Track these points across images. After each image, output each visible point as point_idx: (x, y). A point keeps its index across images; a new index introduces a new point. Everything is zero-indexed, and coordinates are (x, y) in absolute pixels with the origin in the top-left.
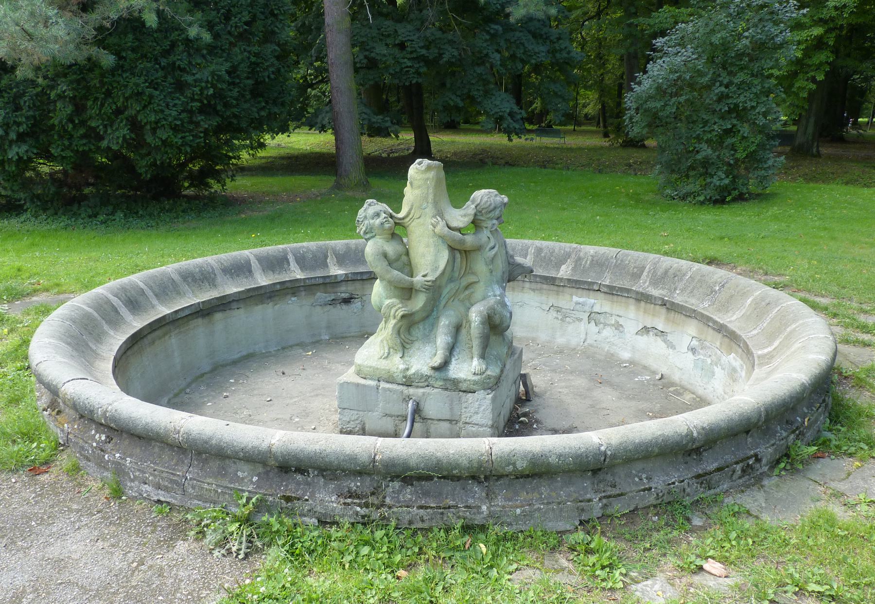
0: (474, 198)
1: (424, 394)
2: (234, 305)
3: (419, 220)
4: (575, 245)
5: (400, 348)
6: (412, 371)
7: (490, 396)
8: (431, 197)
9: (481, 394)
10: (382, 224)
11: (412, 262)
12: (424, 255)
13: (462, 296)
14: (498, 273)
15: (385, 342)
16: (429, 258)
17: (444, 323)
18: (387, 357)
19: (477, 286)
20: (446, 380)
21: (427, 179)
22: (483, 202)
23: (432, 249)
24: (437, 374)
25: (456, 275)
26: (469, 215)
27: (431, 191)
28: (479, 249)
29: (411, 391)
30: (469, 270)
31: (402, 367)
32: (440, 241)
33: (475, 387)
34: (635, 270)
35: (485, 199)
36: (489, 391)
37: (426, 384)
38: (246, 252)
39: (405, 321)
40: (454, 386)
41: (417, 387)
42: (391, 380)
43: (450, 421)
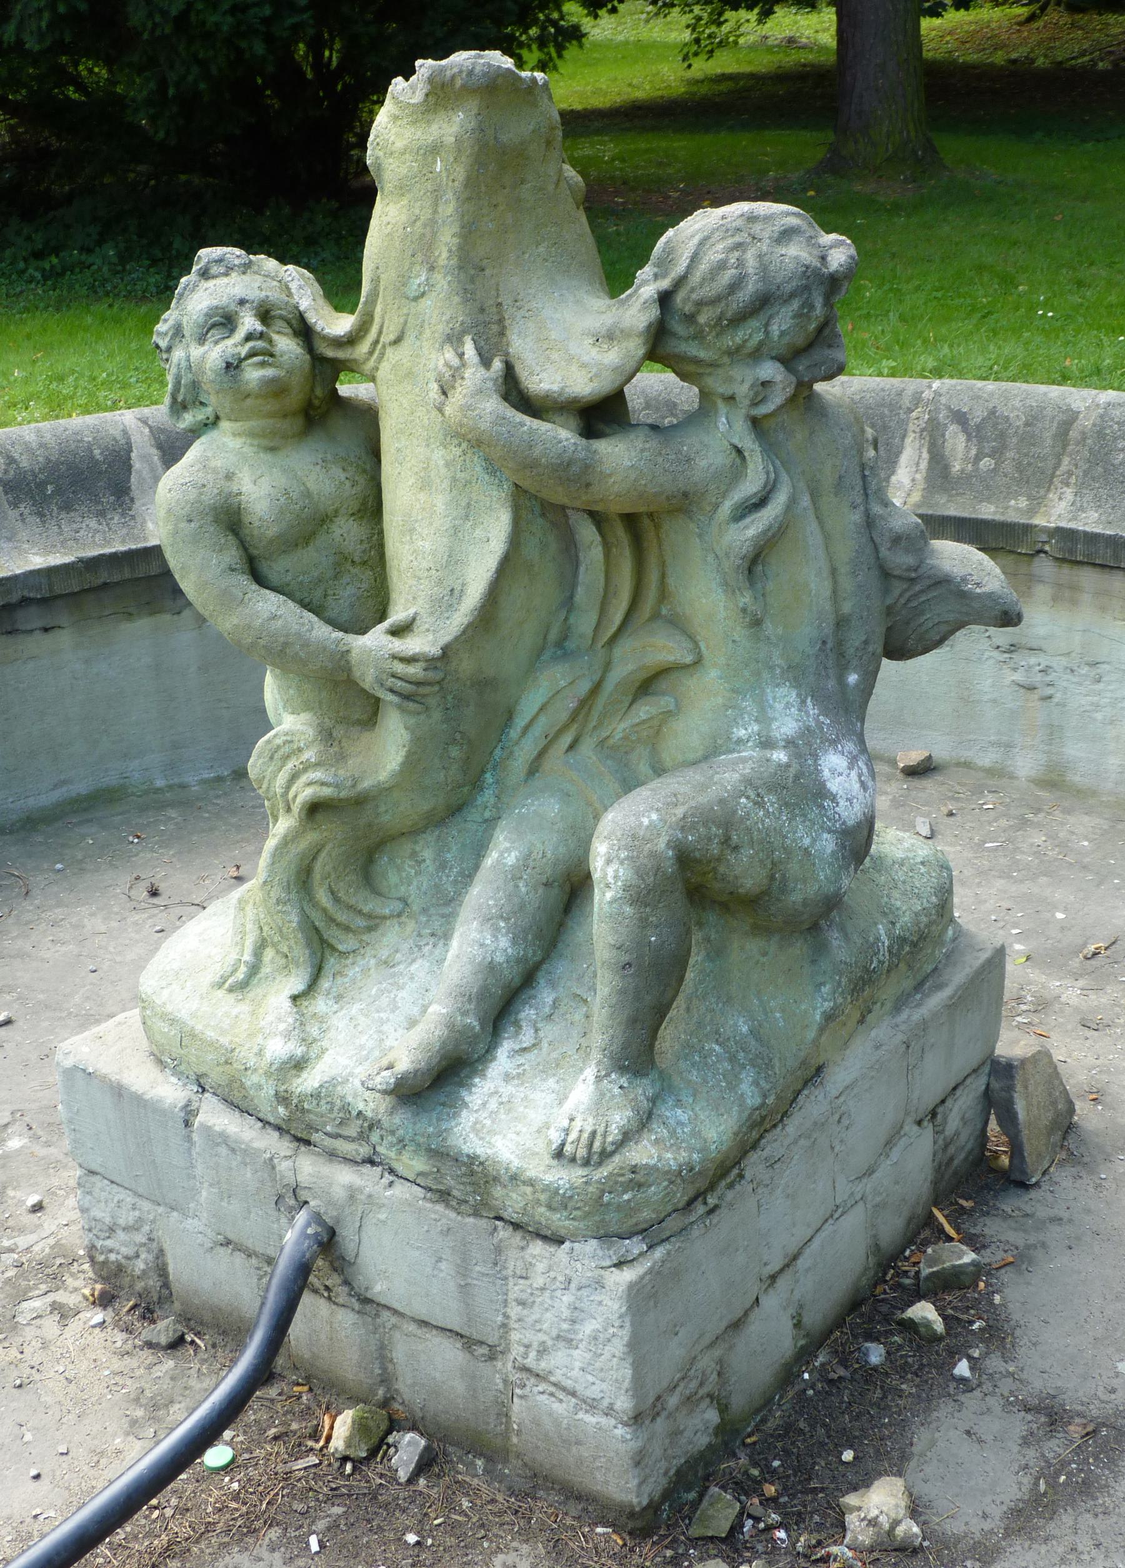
0: (669, 251)
1: (352, 1194)
2: (31, 618)
5: (301, 953)
6: (308, 1082)
7: (628, 1275)
8: (447, 239)
9: (585, 1256)
10: (232, 367)
13: (619, 728)
14: (806, 628)
17: (508, 853)
18: (243, 986)
19: (690, 684)
20: (441, 1154)
21: (435, 149)
22: (703, 267)
23: (440, 501)
24: (401, 1120)
25: (584, 623)
26: (626, 334)
27: (449, 209)
28: (684, 504)
29: (307, 1168)
30: (648, 600)
33: (558, 1221)
35: (714, 255)
36: (635, 1246)
37: (364, 1151)
38: (128, 418)
39: (330, 830)
40: (467, 1187)
41: (332, 1155)
43: (469, 1343)
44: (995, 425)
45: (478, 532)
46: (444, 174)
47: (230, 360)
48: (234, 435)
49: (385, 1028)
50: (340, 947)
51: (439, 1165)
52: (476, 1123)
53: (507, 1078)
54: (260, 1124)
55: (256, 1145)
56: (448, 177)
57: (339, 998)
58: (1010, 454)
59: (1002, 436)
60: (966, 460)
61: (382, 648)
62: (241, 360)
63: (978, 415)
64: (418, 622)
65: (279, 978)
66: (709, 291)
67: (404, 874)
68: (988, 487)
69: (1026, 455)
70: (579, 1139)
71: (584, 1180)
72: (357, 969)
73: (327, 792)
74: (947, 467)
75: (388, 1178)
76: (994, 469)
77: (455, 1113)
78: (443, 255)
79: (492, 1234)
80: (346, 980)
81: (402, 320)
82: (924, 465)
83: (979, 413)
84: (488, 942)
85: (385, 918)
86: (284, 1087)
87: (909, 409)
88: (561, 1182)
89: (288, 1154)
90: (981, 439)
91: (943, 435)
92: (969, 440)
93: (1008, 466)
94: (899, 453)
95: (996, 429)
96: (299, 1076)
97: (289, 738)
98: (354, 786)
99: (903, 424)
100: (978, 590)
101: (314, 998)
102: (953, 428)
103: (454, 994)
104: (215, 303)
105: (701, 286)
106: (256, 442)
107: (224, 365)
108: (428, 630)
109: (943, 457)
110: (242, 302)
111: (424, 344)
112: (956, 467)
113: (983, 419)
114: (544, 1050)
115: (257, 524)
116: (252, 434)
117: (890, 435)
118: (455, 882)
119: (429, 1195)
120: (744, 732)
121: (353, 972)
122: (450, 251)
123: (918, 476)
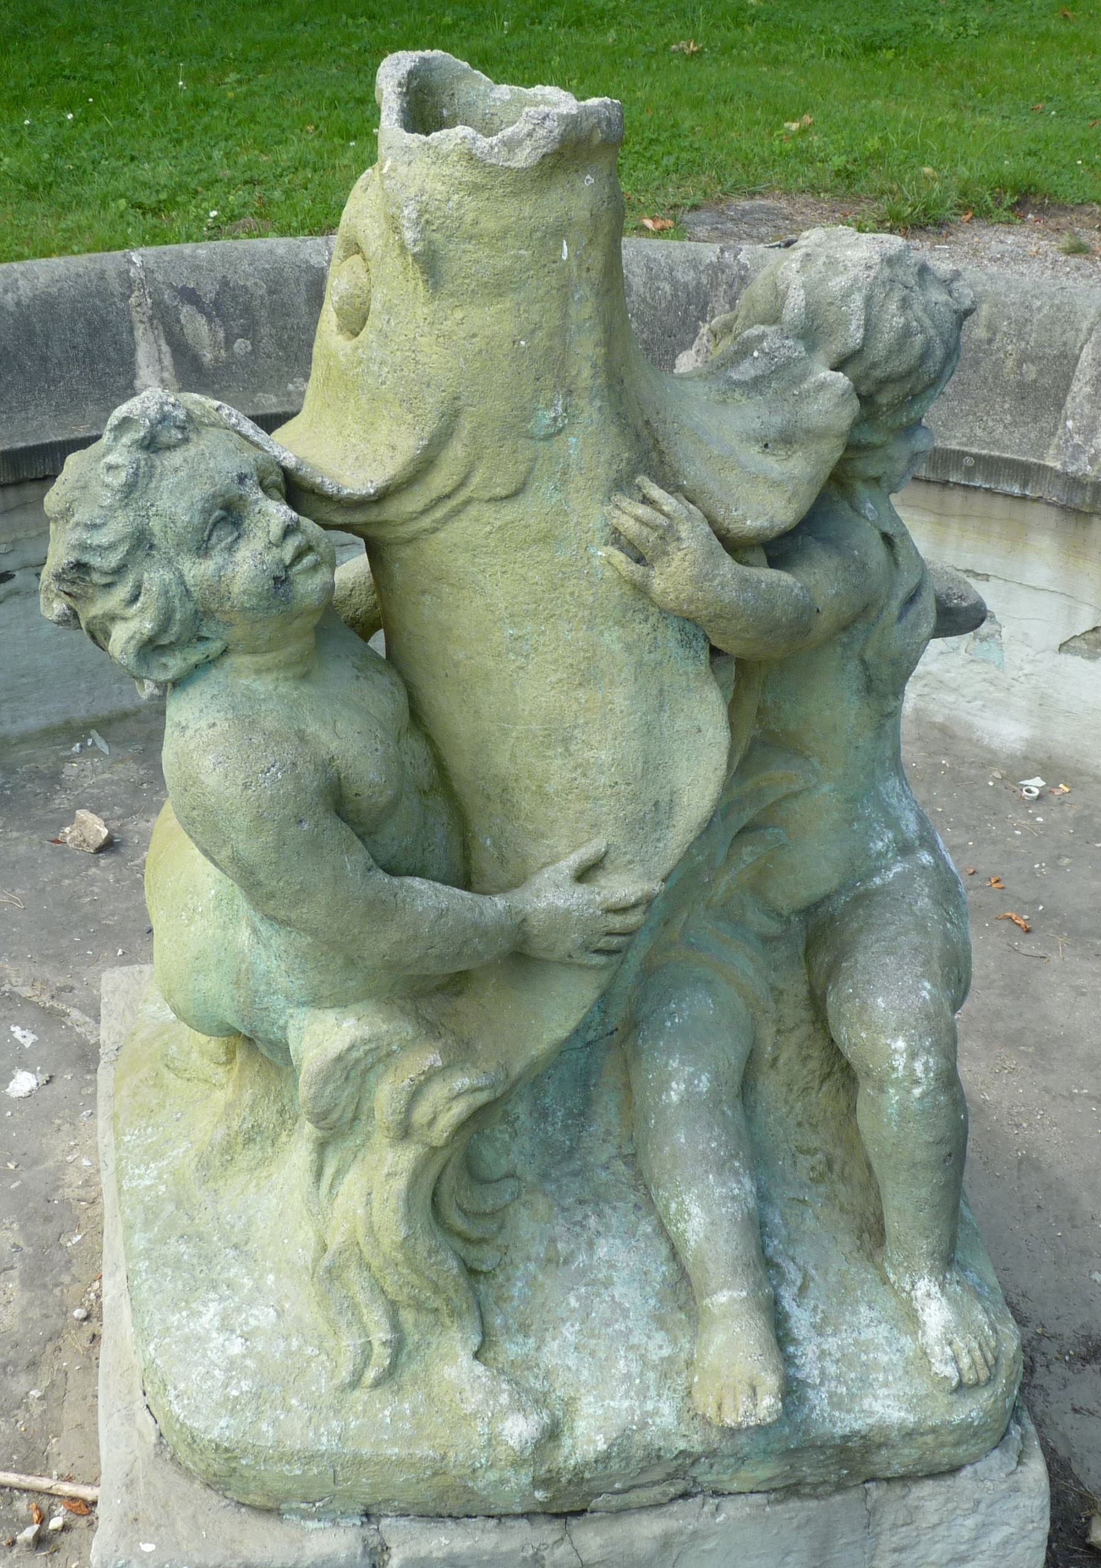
1: (666, 1542)
3: (509, 512)
4: (710, 252)
11: (460, 765)
12: (558, 736)
15: (356, 1282)
16: (604, 752)
18: (390, 1375)
21: (558, 232)
22: (886, 337)
23: (620, 698)
26: (814, 435)
31: (519, 1429)
32: (670, 637)
34: (1031, 371)
37: (680, 1486)
42: (452, 1505)
44: (234, 298)
45: (681, 724)
46: (574, 264)
47: (278, 574)
48: (258, 672)
49: (634, 1340)
50: (484, 1268)
51: (792, 1461)
52: (830, 1397)
53: (819, 1329)
54: (493, 1522)
55: (504, 1548)
56: (579, 266)
57: (524, 1329)
58: (265, 330)
59: (247, 310)
60: (215, 345)
61: (589, 903)
62: (287, 568)
63: (209, 291)
64: (612, 856)
65: (434, 1340)
66: (898, 365)
67: (498, 1144)
68: (253, 374)
69: (284, 328)
70: (974, 1362)
71: (992, 1400)
72: (520, 1284)
73: (482, 1097)
74: (196, 359)
75: (713, 1502)
76: (253, 350)
77: (799, 1398)
78: (584, 371)
79: (865, 1500)
80: (515, 1303)
81: (522, 468)
82: (167, 360)
83: (209, 287)
84: (736, 1191)
85: (506, 1206)
86: (545, 1468)
87: (123, 294)
88: (974, 1414)
89: (557, 1537)
90: (224, 318)
91: (178, 321)
92: (210, 321)
93: (267, 345)
94: (133, 352)
95: (237, 303)
96: (559, 1447)
97: (373, 1045)
98: (507, 1076)
99: (124, 313)
100: (964, 604)
101: (496, 1343)
102: (186, 311)
103: (739, 1270)
105: (887, 359)
107: (271, 582)
108: (631, 862)
109: (186, 346)
110: (242, 479)
111: (573, 496)
112: (208, 356)
113: (218, 294)
114: (817, 1278)
116: (288, 665)
117: (114, 330)
118: (566, 1127)
119: (772, 1496)
120: (881, 844)
121: (517, 1289)
122: (594, 366)
123: (166, 375)
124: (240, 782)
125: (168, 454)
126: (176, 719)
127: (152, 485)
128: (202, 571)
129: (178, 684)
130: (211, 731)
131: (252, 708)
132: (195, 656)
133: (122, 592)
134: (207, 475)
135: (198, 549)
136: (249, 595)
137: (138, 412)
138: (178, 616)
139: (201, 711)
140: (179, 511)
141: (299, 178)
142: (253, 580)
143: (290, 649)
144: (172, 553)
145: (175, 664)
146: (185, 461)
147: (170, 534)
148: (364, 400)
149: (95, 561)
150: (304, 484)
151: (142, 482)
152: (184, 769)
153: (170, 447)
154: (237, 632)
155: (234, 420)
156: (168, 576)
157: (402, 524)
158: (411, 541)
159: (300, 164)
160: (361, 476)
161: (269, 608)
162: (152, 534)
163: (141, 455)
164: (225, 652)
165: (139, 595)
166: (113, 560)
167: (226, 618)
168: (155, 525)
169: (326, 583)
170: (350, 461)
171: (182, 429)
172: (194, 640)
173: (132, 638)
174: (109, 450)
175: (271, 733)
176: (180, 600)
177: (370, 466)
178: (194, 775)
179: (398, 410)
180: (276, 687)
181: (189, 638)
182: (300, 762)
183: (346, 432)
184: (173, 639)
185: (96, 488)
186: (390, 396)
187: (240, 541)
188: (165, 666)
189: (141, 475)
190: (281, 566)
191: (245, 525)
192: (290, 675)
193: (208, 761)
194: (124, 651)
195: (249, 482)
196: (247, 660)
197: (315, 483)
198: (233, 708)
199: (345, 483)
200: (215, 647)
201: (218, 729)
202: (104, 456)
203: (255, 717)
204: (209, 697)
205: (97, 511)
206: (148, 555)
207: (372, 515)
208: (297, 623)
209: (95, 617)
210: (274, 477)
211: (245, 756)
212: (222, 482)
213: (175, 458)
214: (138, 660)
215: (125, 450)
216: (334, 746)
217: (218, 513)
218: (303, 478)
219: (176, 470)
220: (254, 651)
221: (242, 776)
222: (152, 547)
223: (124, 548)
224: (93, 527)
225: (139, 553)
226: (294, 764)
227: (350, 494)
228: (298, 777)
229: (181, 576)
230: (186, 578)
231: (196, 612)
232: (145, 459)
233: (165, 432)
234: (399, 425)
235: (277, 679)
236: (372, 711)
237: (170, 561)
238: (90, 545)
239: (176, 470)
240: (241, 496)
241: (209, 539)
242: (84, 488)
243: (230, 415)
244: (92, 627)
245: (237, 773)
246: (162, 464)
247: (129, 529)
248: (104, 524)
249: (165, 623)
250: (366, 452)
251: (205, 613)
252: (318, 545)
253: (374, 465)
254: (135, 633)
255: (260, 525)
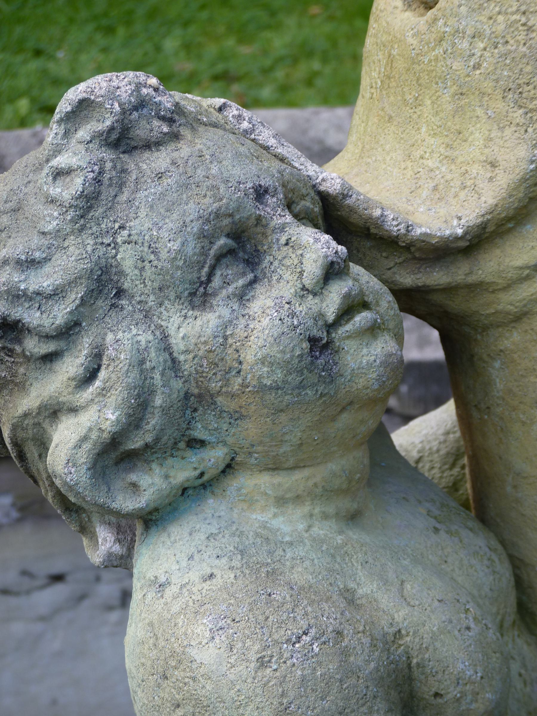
47: (315, 333)
48: (281, 501)
62: (331, 327)
104: (209, 204)
106: (331, 510)
107: (306, 345)
115: (454, 692)
116: (327, 493)
124: (253, 656)
125: (147, 154)
126: (150, 575)
127: (124, 197)
128: (197, 328)
129: (152, 519)
130: (206, 586)
131: (270, 553)
132: (182, 472)
133: (72, 365)
134: (209, 183)
135: (193, 294)
136: (271, 364)
137: (102, 92)
138: (158, 401)
139: (191, 558)
140: (164, 233)
141: (302, 70)
142: (277, 340)
143: (333, 466)
144: (151, 300)
145: (151, 484)
146: (173, 163)
147: (149, 272)
148: (447, 98)
149: (32, 317)
150: (354, 219)
151: (107, 193)
152: (161, 643)
153: (149, 145)
154: (250, 430)
155: (245, 125)
156: (145, 337)
157: (507, 288)
158: (519, 317)
159: (304, 51)
160: (442, 212)
161: (301, 386)
162: (121, 273)
163: (108, 155)
164: (229, 468)
165: (98, 370)
166: (59, 314)
167: (233, 405)
168: (127, 258)
169: (390, 355)
170: (425, 193)
171: (170, 121)
172: (182, 445)
173: (85, 439)
174: (57, 151)
175: (302, 588)
176: (162, 375)
177: (456, 196)
178: (179, 650)
179: (500, 105)
180: (310, 527)
181: (177, 443)
182: (348, 631)
183: (417, 154)
184: (149, 438)
185: (36, 207)
186: (488, 85)
187: (257, 286)
188: (134, 486)
189: (106, 182)
190: (320, 323)
191: (265, 263)
192: (331, 510)
193: (202, 628)
194: (70, 461)
195: (271, 200)
196: (262, 482)
197: (371, 218)
198: (242, 553)
199: (418, 221)
200: (214, 457)
201: (218, 581)
202: (48, 161)
203: (277, 566)
204: (203, 537)
205: (36, 241)
206: (113, 306)
207: (458, 273)
208: (345, 418)
209: (26, 415)
210: (307, 203)
211: (261, 618)
212: (229, 197)
213: (160, 159)
214: (93, 477)
215: (82, 148)
216: (401, 615)
217: (222, 241)
218: (352, 210)
219: (160, 176)
220: (275, 467)
221: (257, 647)
222: (120, 293)
223: (75, 296)
224: (30, 264)
225: (100, 303)
226: (339, 633)
227: (426, 234)
228: (345, 653)
229: (165, 337)
230: (173, 341)
231: (187, 396)
232: (112, 160)
233: (143, 123)
234: (501, 129)
235: (311, 515)
236: (459, 579)
237: (148, 315)
238: (25, 291)
239: (160, 176)
240: (259, 219)
241: (209, 280)
242: (15, 211)
243: (239, 117)
244: (21, 434)
245: (248, 643)
246: (139, 168)
247: (86, 265)
248: (47, 260)
249: (138, 410)
250: (449, 177)
251: (200, 397)
252: (377, 304)
253: (462, 195)
254: (90, 429)
255: (287, 262)
